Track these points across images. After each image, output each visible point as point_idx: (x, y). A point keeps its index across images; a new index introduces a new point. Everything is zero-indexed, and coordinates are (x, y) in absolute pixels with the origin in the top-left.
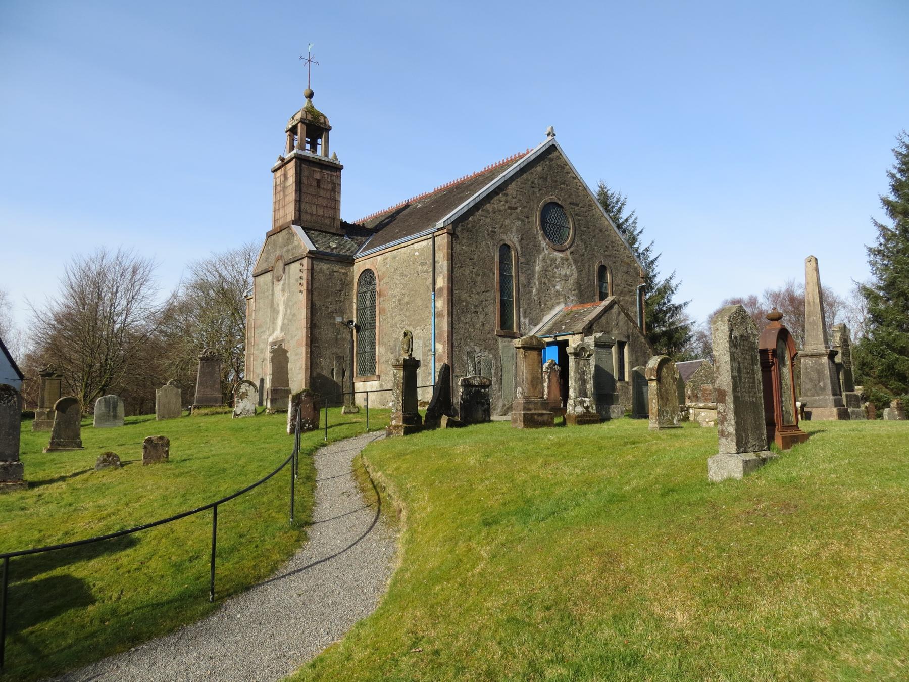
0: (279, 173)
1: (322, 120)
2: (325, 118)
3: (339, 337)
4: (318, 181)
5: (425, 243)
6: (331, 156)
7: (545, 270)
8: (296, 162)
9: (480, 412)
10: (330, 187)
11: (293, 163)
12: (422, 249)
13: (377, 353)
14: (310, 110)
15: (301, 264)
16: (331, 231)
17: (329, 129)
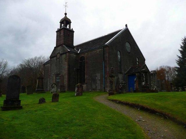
0: (58, 33)
5: (101, 49)
6: (71, 29)
13: (86, 77)
17: (71, 22)
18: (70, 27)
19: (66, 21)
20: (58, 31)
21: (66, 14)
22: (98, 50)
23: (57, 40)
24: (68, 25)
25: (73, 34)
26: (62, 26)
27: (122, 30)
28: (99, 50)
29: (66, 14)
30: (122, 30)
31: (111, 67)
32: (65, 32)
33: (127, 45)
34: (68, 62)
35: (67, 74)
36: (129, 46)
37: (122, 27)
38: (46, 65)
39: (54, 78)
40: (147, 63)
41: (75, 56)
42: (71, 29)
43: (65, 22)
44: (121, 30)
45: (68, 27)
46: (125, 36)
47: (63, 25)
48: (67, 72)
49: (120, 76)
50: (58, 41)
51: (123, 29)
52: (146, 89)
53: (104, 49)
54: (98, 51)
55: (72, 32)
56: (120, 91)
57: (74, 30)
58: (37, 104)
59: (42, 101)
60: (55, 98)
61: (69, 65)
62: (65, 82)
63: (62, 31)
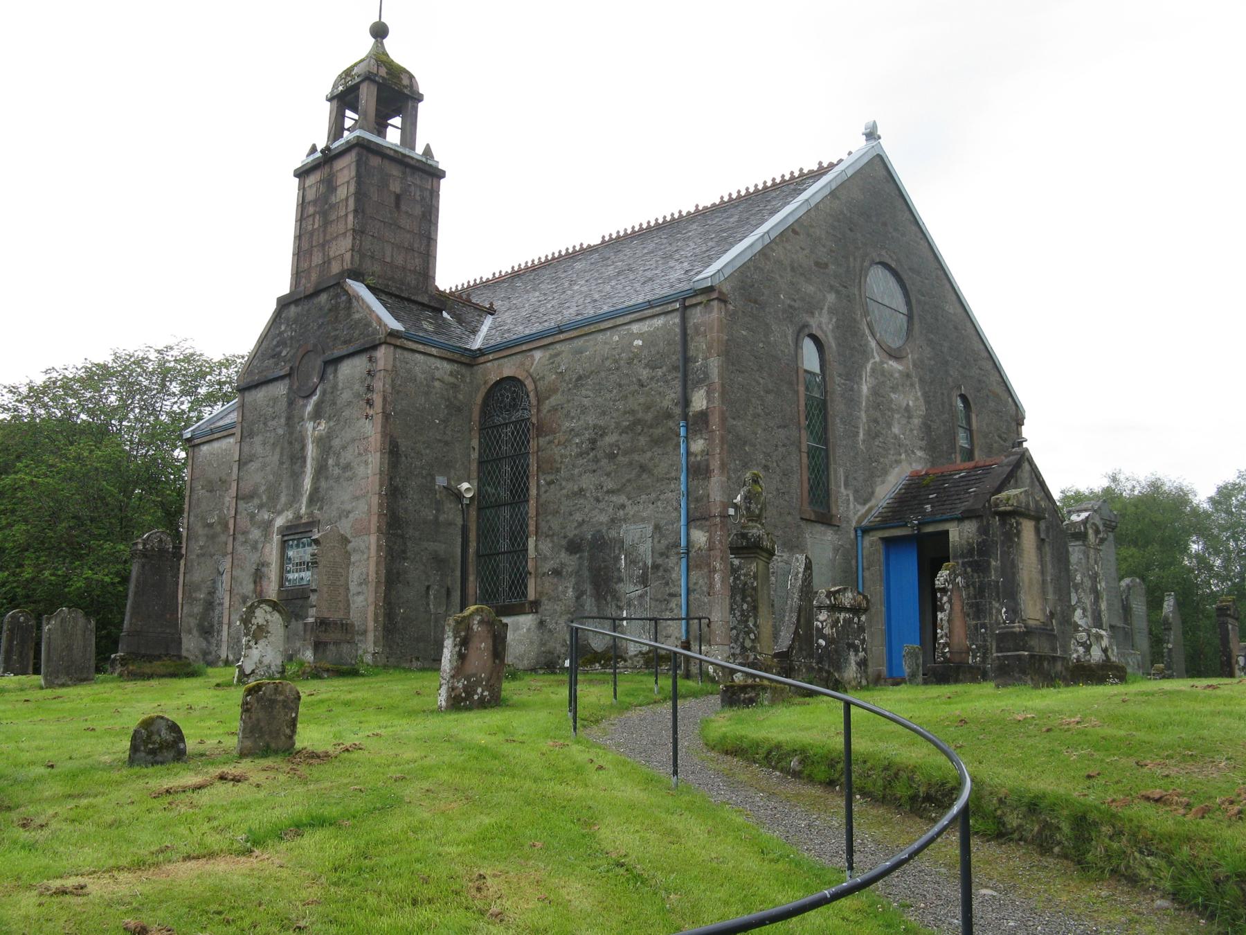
0: (312, 180)
1: (406, 82)
2: (411, 77)
3: (442, 518)
4: (398, 198)
5: (659, 322)
6: (419, 150)
7: (875, 392)
8: (358, 154)
9: (853, 666)
10: (418, 211)
11: (350, 158)
12: (650, 334)
13: (531, 552)
14: (380, 57)
15: (370, 359)
16: (419, 299)
17: (419, 98)
18: (409, 133)
19: (381, 90)
20: (317, 170)
21: (379, 31)
22: (635, 328)
23: (299, 237)
24: (397, 121)
25: (434, 194)
26: (348, 123)
27: (813, 191)
28: (644, 327)
29: (379, 31)
30: (813, 191)
31: (745, 466)
32: (370, 177)
33: (880, 285)
34: (386, 416)
35: (374, 519)
36: (899, 302)
37: (833, 145)
38: (205, 448)
39: (272, 552)
40: (1037, 438)
41: (444, 369)
42: (419, 150)
43: (367, 96)
44: (832, 166)
45: (393, 136)
46: (862, 226)
47: (350, 117)
48: (375, 509)
49: (822, 545)
50: (305, 246)
51: (848, 161)
52: (1031, 659)
53: (684, 320)
54: (640, 336)
55: (427, 174)
56: (814, 662)
57: (442, 159)
58: (110, 767)
59: (157, 745)
60: (269, 725)
61: (393, 452)
62: (353, 588)
63: (340, 164)
